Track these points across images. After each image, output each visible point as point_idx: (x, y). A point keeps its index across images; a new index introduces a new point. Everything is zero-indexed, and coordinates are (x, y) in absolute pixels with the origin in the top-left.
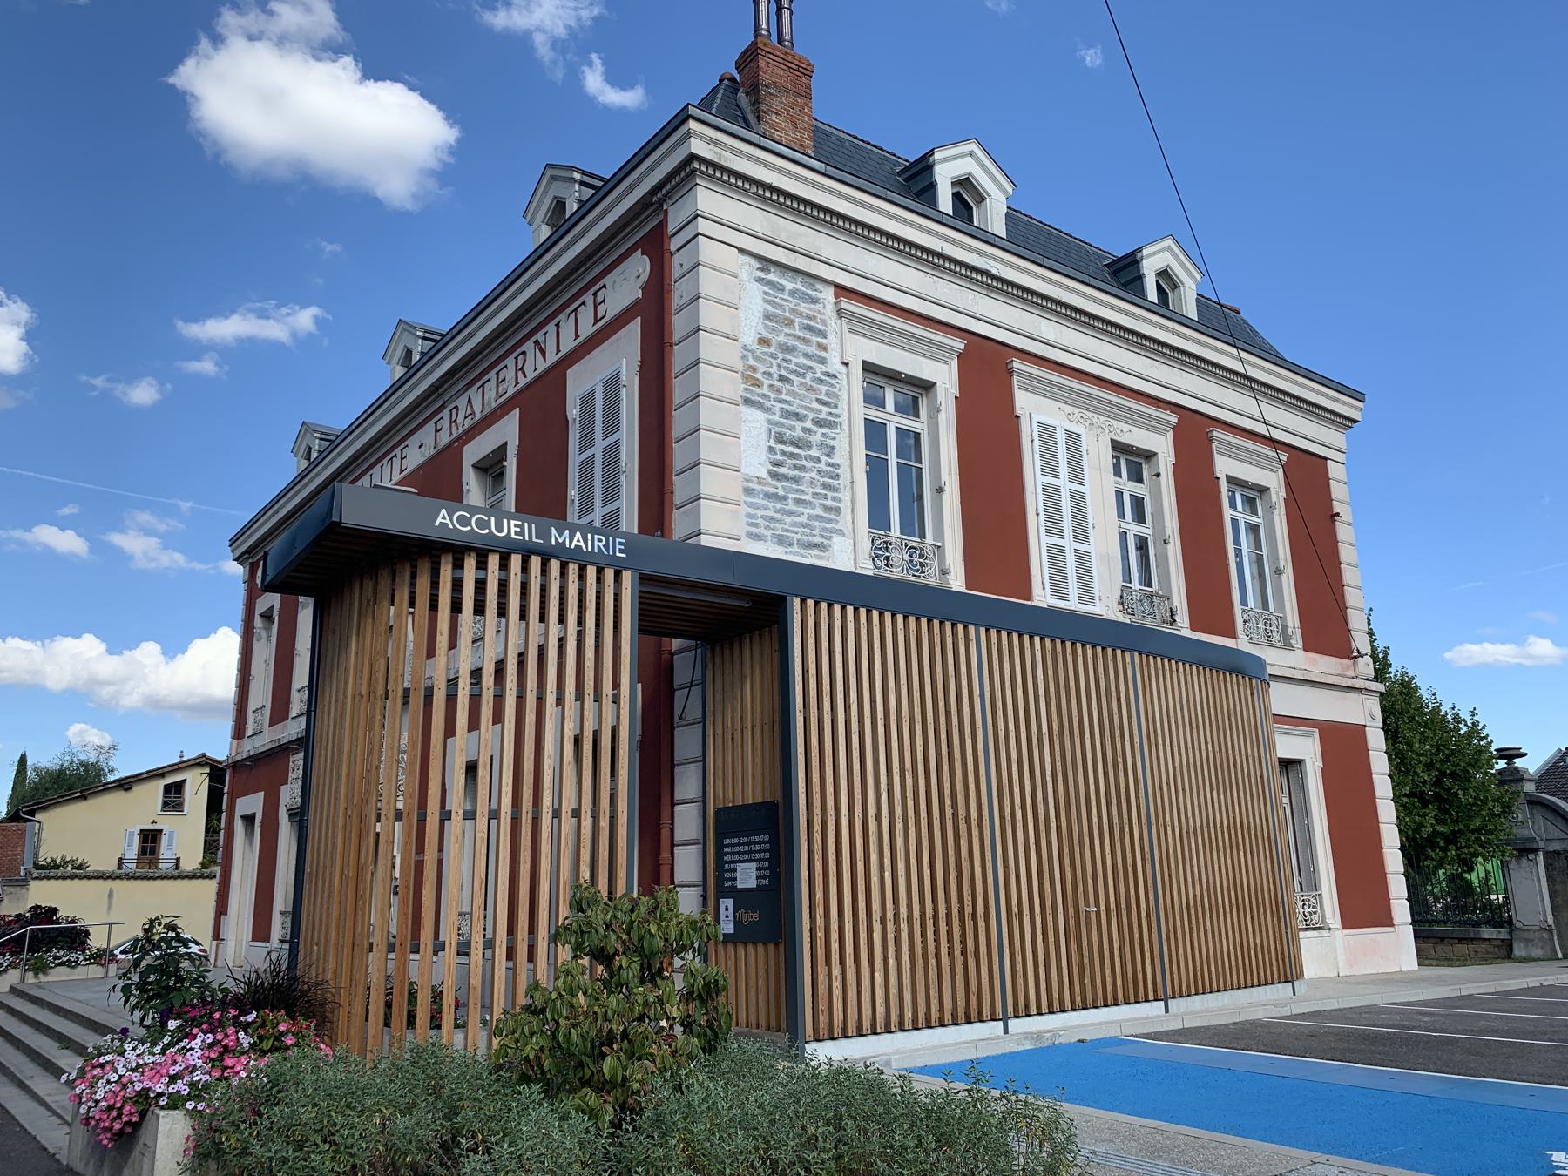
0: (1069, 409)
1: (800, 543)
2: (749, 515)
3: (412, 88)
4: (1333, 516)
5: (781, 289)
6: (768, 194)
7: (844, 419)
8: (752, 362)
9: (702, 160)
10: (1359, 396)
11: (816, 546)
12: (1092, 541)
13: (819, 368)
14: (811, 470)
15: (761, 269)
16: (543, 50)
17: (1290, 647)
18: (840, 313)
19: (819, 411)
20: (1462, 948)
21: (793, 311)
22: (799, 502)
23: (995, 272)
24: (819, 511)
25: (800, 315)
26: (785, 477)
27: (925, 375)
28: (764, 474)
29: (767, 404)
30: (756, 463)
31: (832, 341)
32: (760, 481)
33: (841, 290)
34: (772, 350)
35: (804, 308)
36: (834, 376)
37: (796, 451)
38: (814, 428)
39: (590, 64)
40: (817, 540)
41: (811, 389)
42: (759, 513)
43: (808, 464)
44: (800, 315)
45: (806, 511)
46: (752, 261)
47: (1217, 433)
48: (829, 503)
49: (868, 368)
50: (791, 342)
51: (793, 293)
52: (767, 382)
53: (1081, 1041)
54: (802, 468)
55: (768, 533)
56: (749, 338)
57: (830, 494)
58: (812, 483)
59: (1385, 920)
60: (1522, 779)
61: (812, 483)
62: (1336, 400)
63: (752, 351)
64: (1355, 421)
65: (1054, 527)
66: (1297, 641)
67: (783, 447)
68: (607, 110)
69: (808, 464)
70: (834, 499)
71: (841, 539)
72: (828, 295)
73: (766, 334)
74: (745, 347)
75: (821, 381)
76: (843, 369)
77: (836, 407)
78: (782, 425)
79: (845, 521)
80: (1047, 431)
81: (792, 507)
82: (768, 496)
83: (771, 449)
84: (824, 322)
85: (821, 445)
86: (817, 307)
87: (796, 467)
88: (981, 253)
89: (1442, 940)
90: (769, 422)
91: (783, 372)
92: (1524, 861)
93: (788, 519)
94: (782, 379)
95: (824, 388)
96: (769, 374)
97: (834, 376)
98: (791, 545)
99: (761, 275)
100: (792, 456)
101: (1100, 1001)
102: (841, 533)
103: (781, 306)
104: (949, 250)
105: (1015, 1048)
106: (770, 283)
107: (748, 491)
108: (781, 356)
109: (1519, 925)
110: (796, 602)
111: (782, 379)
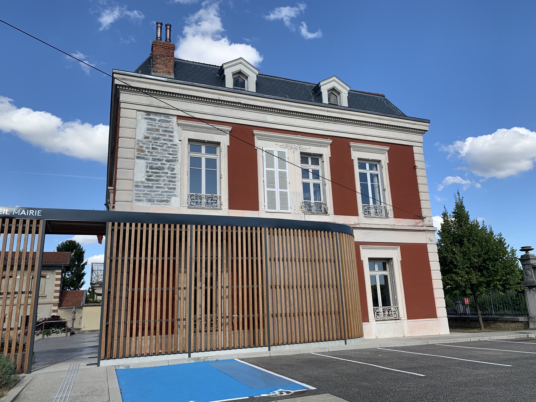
0: (281, 144)
1: (157, 201)
2: (136, 194)
3: (247, 44)
4: (415, 167)
5: (155, 120)
6: (147, 91)
7: (179, 159)
8: (141, 145)
9: (120, 85)
10: (428, 122)
11: (164, 201)
12: (288, 188)
13: (169, 144)
14: (164, 176)
15: (147, 115)
16: (287, 23)
17: (387, 216)
18: (178, 125)
19: (169, 157)
20: (513, 325)
21: (159, 126)
22: (158, 187)
23: (243, 102)
24: (166, 190)
25: (162, 127)
26: (153, 180)
27: (216, 140)
28: (143, 180)
29: (147, 157)
30: (140, 175)
31: (175, 134)
32: (142, 182)
33: (179, 117)
34: (150, 140)
35: (164, 125)
36: (176, 145)
37: (158, 171)
38: (166, 163)
39: (302, 25)
40: (165, 199)
41: (166, 150)
42: (141, 192)
43: (162, 175)
44: (162, 127)
45: (161, 190)
46: (143, 113)
47: (352, 144)
48: (171, 186)
49: (190, 140)
50: (157, 136)
51: (159, 121)
52: (147, 150)
53: (217, 360)
54: (160, 176)
55: (144, 199)
56: (140, 137)
57: (171, 183)
58: (164, 181)
59: (432, 314)
60: (530, 259)
61: (164, 181)
62: (415, 124)
63: (141, 141)
64: (426, 131)
65: (271, 183)
66: (391, 214)
67: (153, 171)
68: (310, 40)
69: (162, 175)
70: (173, 185)
71: (175, 198)
72: (175, 119)
73: (147, 135)
74: (138, 141)
75: (170, 147)
76: (180, 142)
77: (176, 155)
78: (152, 163)
79: (177, 192)
80: (270, 153)
81: (155, 189)
82: (145, 187)
83: (147, 172)
84: (172, 128)
85: (169, 168)
86: (170, 123)
87: (157, 176)
88: (236, 97)
89: (506, 322)
90: (147, 163)
91: (154, 146)
92: (532, 291)
93: (153, 194)
94: (153, 148)
95: (171, 149)
96: (148, 148)
97: (176, 145)
98: (154, 201)
99: (147, 117)
100: (156, 173)
101: (262, 345)
102: (175, 196)
103: (154, 125)
104: (222, 98)
105: (192, 361)
106: (151, 119)
107: (137, 186)
108: (153, 141)
109: (531, 316)
110: (110, 224)
111: (153, 148)
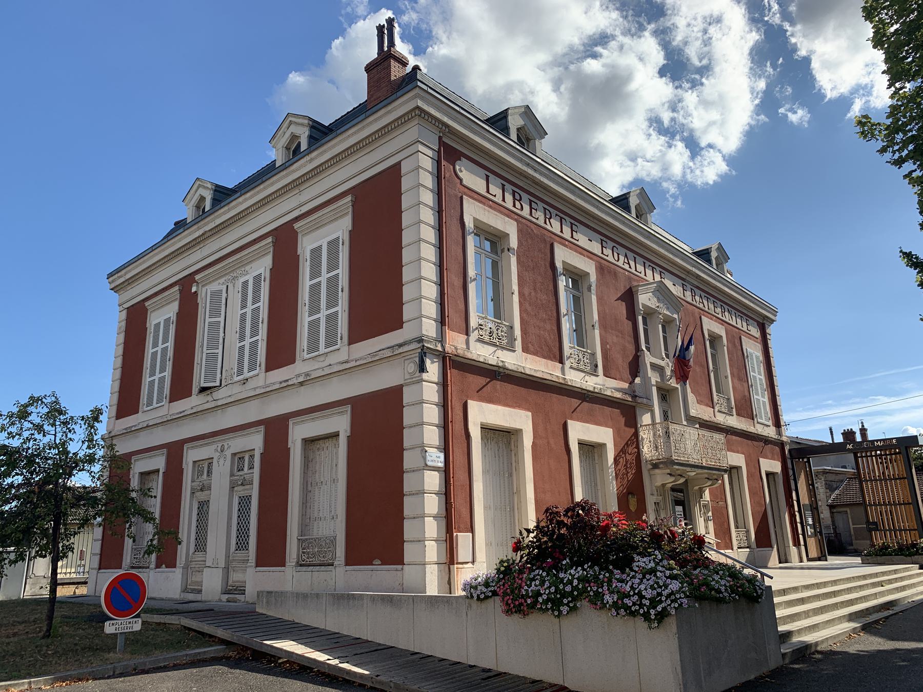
66: (770, 423)
